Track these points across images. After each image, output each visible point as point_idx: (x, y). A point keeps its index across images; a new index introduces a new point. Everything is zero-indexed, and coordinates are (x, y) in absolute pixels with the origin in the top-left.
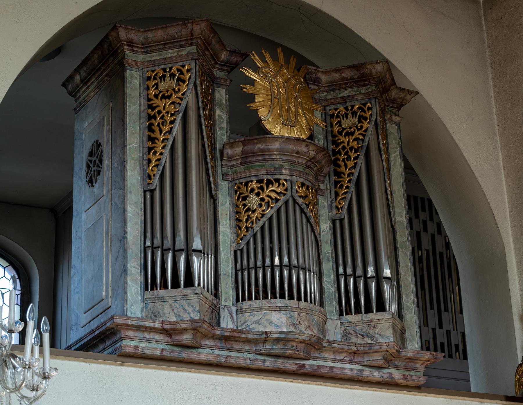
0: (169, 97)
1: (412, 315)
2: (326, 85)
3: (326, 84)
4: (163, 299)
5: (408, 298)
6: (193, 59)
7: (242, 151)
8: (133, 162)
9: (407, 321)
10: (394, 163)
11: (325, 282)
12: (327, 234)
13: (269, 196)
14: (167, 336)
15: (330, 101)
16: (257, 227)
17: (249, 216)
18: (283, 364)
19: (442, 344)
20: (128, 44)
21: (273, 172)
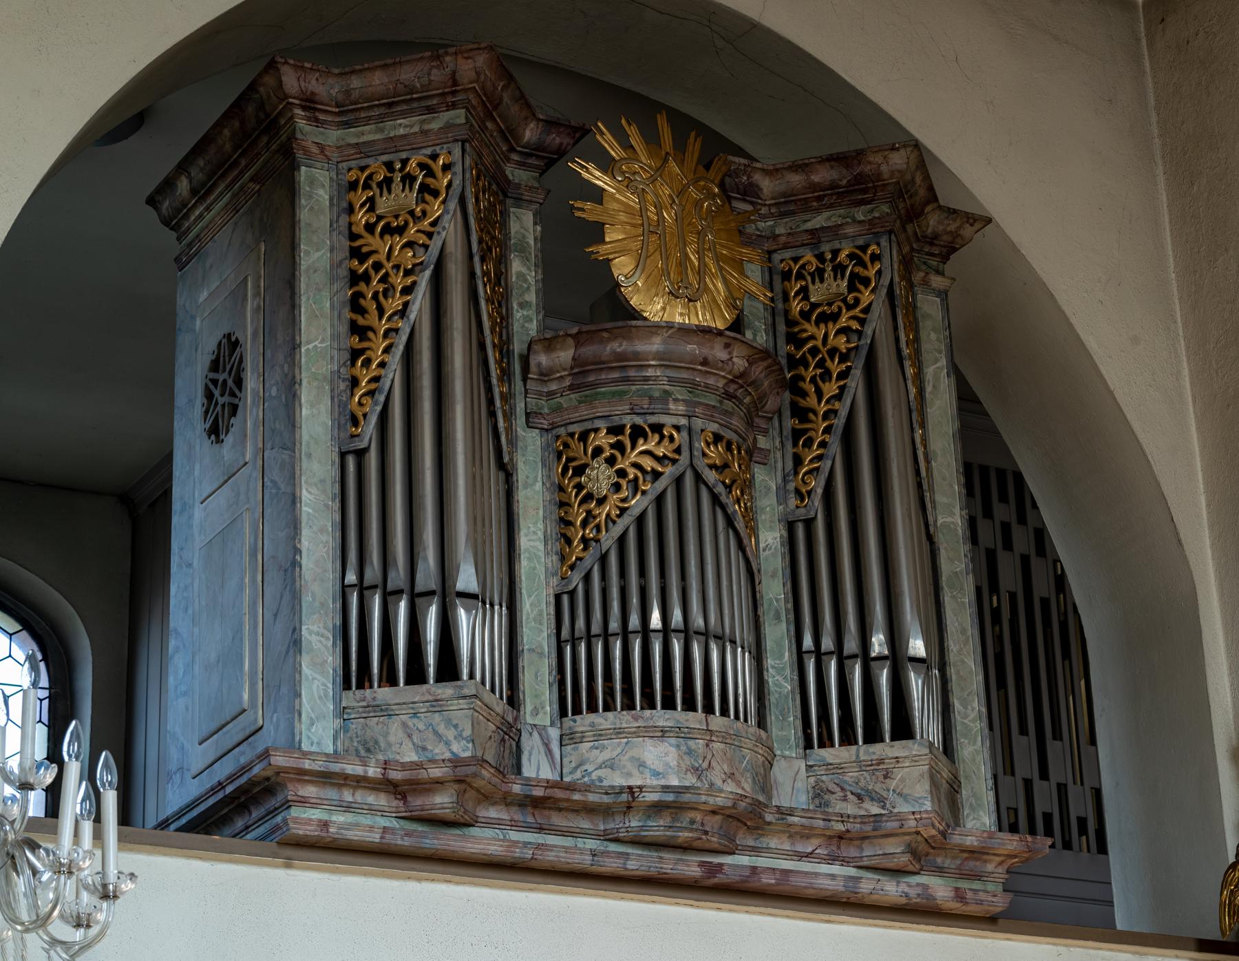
0: (401, 230)
1: (975, 747)
2: (773, 201)
3: (772, 199)
4: (387, 709)
5: (966, 708)
6: (457, 140)
7: (574, 359)
8: (315, 384)
9: (964, 761)
10: (934, 387)
11: (770, 670)
12: (774, 555)
13: (636, 466)
14: (396, 798)
15: (783, 239)
16: (608, 540)
17: (589, 512)
18: (670, 864)
19: (1047, 817)
20: (303, 103)
21: (648, 409)
